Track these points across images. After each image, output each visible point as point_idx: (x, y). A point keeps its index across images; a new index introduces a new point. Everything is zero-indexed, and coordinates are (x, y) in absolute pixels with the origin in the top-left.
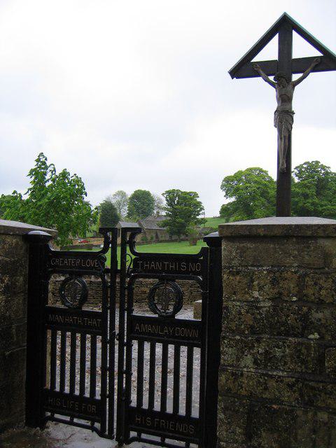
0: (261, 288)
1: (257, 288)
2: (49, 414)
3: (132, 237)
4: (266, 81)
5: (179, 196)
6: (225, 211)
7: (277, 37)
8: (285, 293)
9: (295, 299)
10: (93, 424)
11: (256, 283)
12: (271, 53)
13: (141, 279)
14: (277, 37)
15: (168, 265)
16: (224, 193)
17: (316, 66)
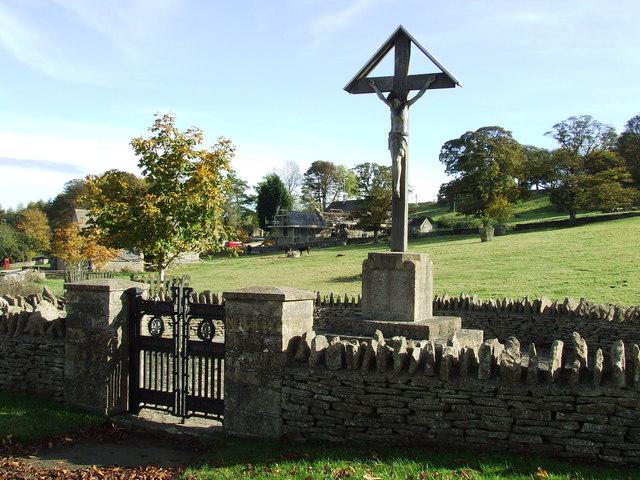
2: (142, 404)
5: (376, 172)
6: (448, 191)
7: (393, 50)
12: (386, 68)
14: (393, 50)
16: (444, 167)
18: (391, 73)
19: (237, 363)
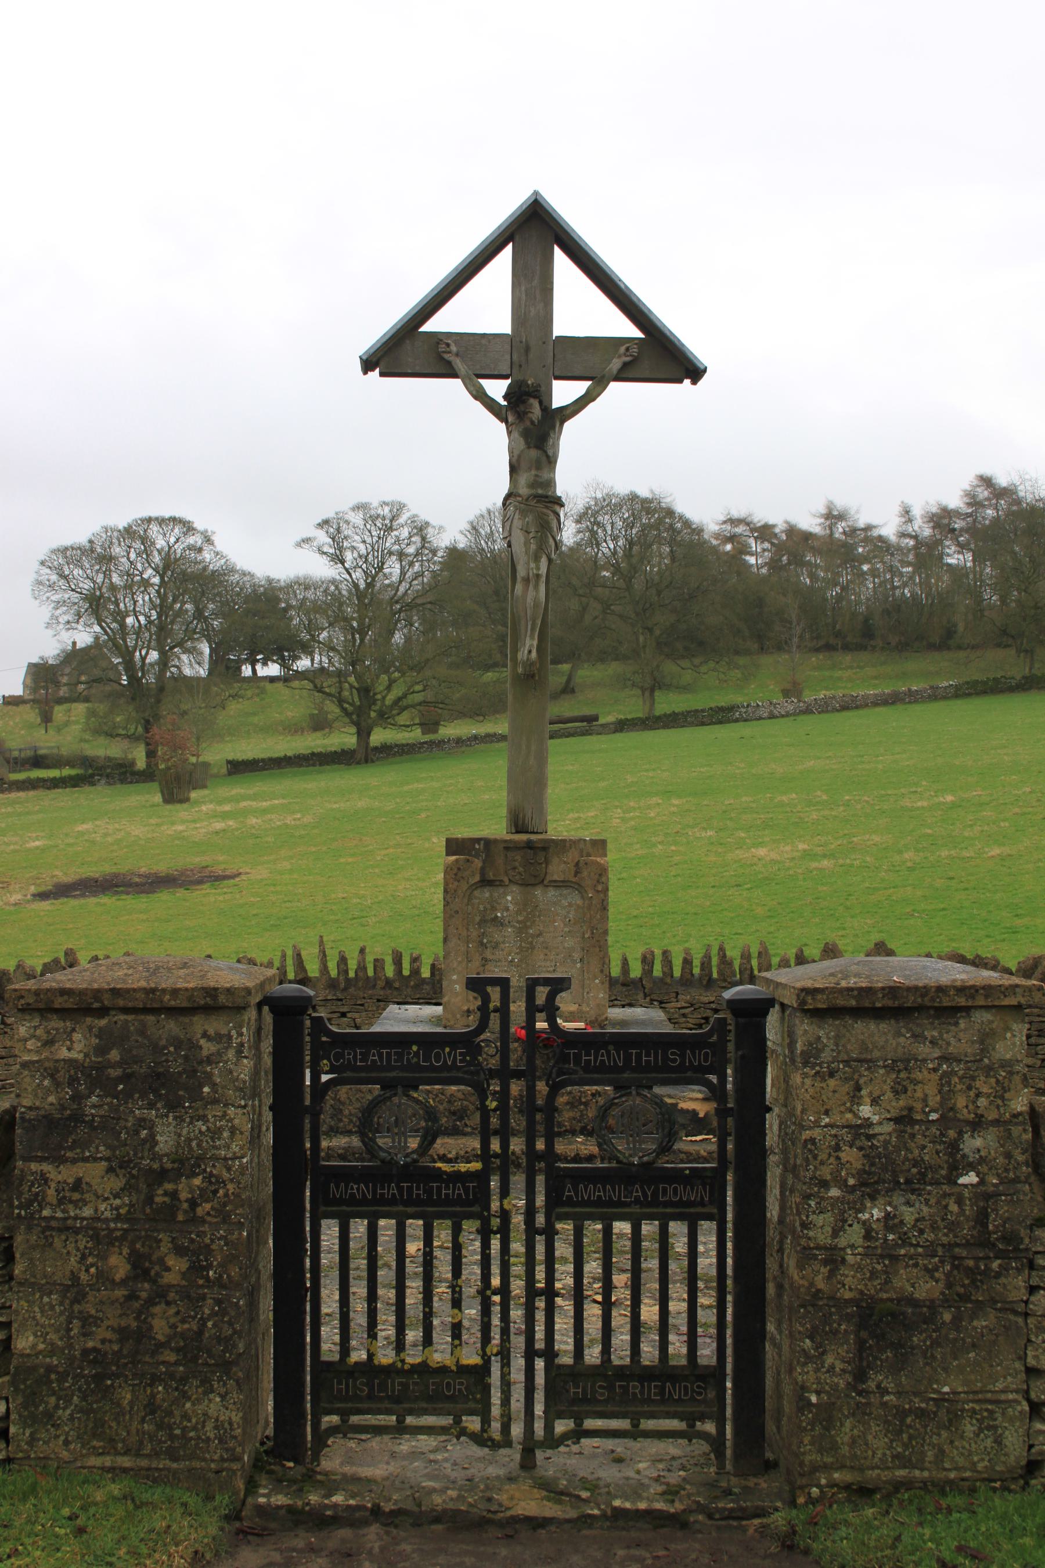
0: (875, 1101)
1: (868, 1100)
3: (551, 997)
4: (476, 398)
8: (918, 1106)
9: (934, 1116)
10: (458, 1421)
11: (864, 1092)
12: (486, 308)
13: (569, 1089)
14: (509, 249)
15: (639, 1056)
17: (625, 365)
18: (561, 327)
19: (854, 1235)
